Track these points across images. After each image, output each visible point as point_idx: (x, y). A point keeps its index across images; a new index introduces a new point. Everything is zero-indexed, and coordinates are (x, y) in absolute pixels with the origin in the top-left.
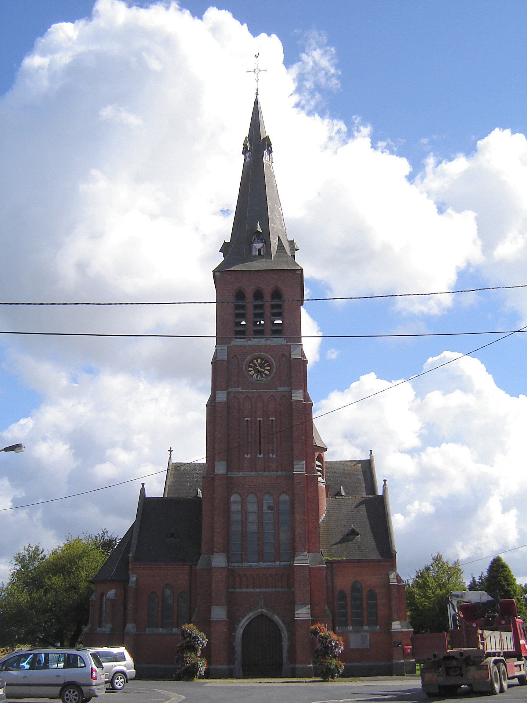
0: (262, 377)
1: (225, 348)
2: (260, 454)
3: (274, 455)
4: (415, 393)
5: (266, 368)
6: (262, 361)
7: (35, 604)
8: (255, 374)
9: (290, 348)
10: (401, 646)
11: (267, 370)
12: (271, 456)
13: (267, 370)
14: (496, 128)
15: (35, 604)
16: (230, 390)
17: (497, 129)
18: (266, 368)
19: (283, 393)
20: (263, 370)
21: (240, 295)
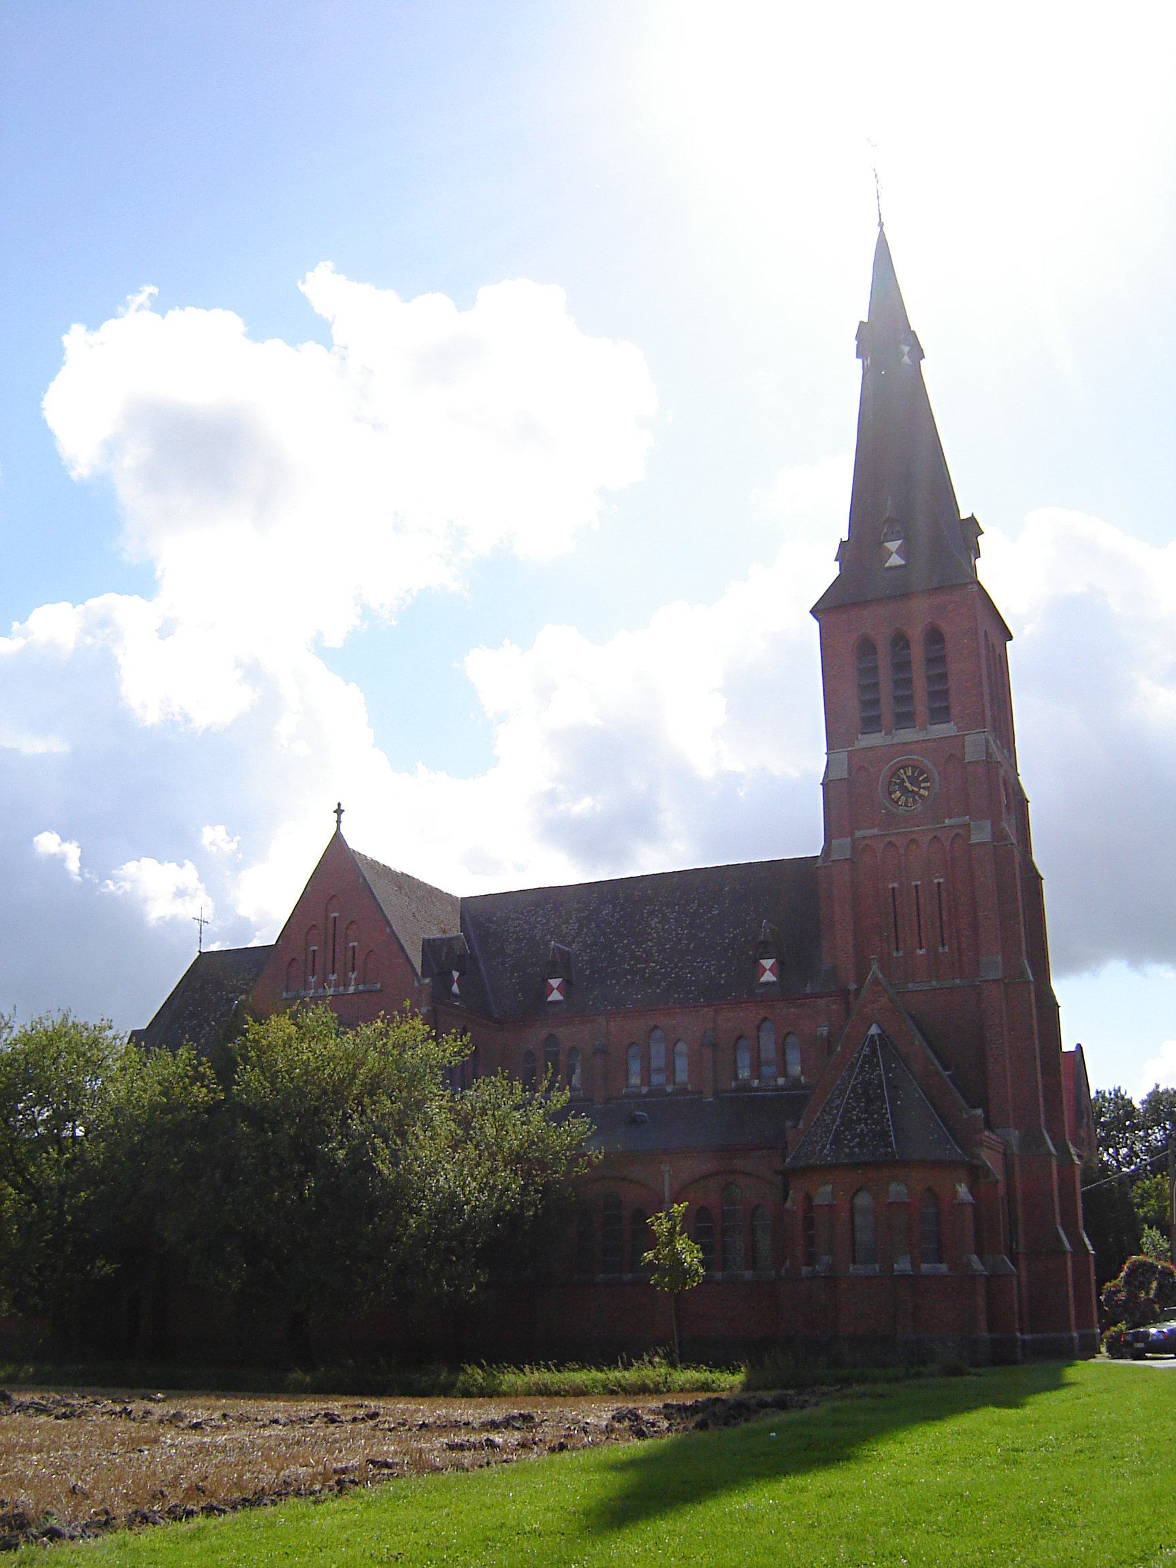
0: (915, 802)
1: (842, 756)
2: (943, 946)
3: (947, 947)
4: (80, 865)
5: (922, 785)
6: (913, 773)
7: (858, 1130)
8: (902, 797)
9: (919, 741)
10: (502, 1227)
11: (923, 788)
12: (940, 949)
13: (923, 788)
14: (61, 343)
15: (858, 1130)
16: (859, 834)
17: (75, 338)
18: (922, 785)
19: (956, 831)
20: (916, 789)
21: (866, 647)
